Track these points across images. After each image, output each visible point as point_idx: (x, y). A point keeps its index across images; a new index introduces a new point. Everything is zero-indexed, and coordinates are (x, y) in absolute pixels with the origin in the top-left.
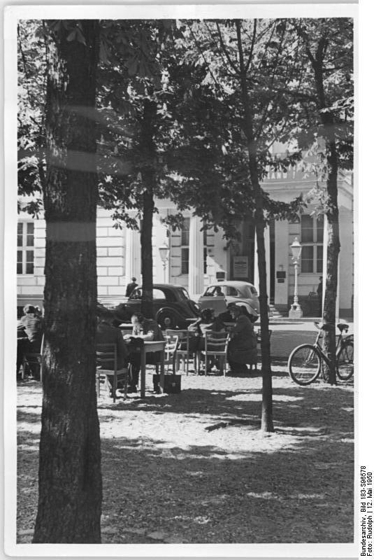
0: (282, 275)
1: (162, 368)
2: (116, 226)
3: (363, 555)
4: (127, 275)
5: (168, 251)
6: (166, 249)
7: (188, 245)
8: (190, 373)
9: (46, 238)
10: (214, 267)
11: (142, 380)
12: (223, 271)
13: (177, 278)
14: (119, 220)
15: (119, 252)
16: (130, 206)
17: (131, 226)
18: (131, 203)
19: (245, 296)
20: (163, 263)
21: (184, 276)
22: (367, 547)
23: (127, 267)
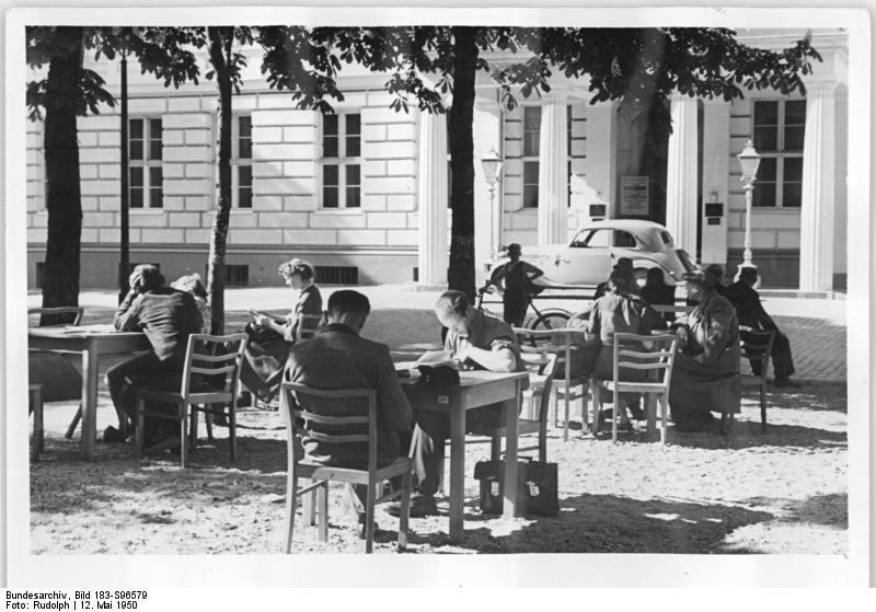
0: (714, 212)
1: (512, 444)
2: (397, 106)
3: (8, 595)
4: (421, 206)
5: (499, 165)
6: (495, 160)
7: (537, 154)
8: (572, 433)
9: (251, 126)
10: (588, 193)
11: (452, 458)
12: (604, 203)
13: (515, 215)
14: (403, 93)
15: (406, 167)
16: (425, 65)
17: (427, 106)
18: (428, 59)
19: (651, 247)
20: (490, 187)
21: (530, 211)
22: (21, 601)
23: (421, 194)
